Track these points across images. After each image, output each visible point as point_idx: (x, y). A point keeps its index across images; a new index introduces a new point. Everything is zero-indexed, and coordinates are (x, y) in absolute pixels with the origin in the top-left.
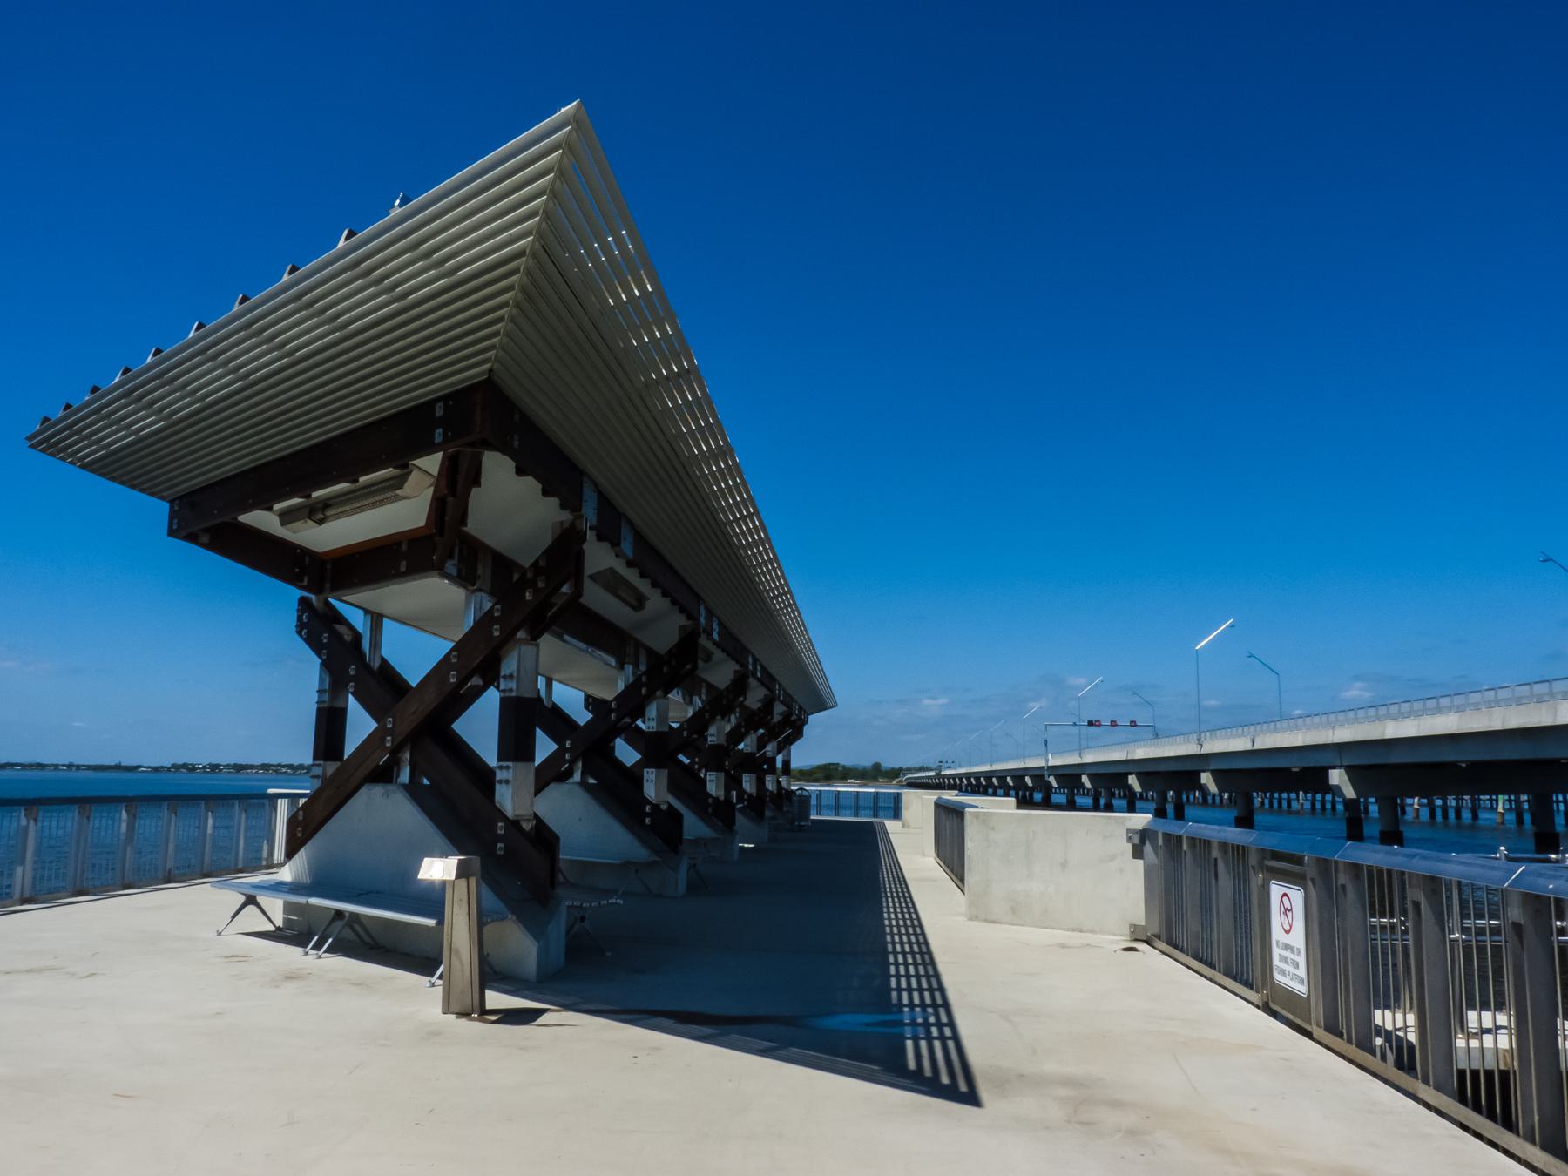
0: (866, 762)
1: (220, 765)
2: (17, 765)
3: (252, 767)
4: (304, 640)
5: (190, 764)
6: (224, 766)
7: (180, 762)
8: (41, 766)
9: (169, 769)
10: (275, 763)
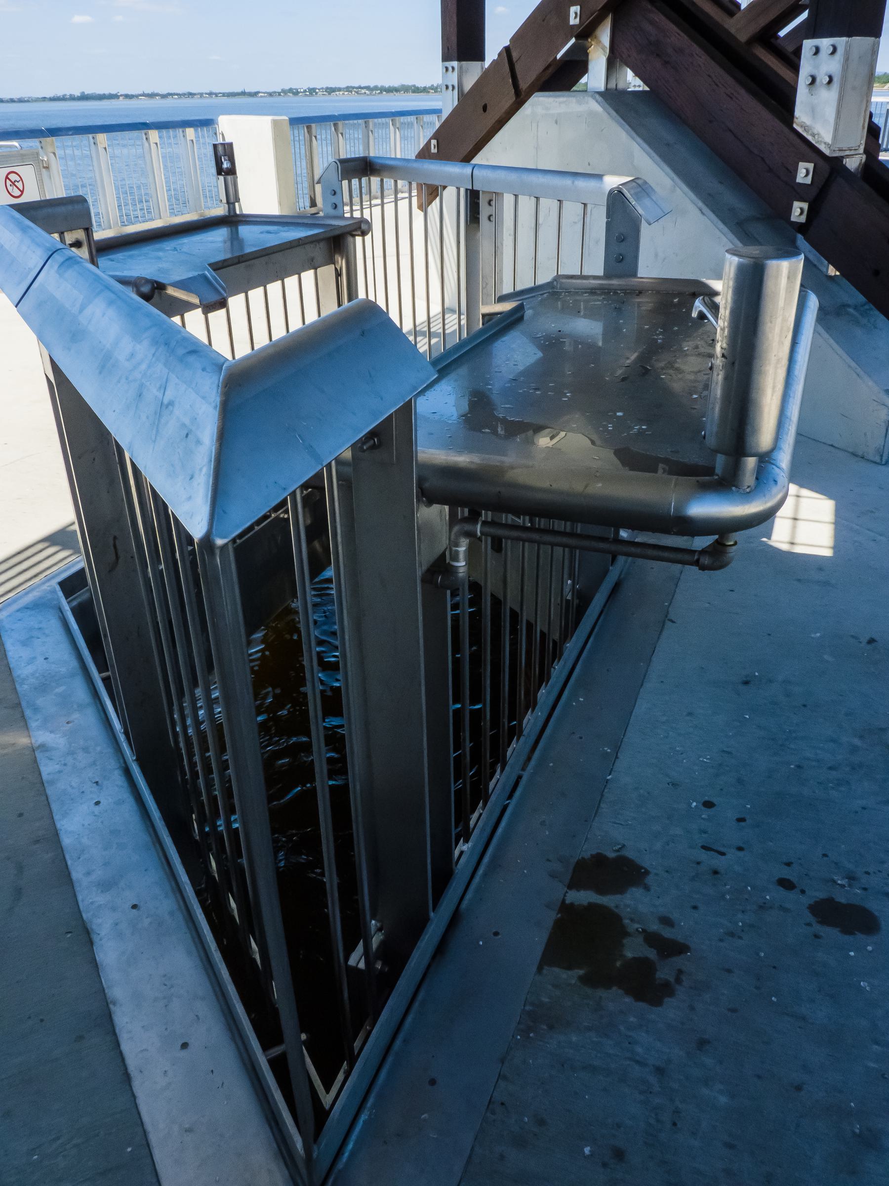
0: (239, 90)
1: (316, 89)
2: (175, 94)
3: (339, 89)
4: (266, 513)
5: (295, 89)
6: (319, 89)
7: (287, 88)
8: (191, 95)
9: (279, 94)
10: (357, 85)
